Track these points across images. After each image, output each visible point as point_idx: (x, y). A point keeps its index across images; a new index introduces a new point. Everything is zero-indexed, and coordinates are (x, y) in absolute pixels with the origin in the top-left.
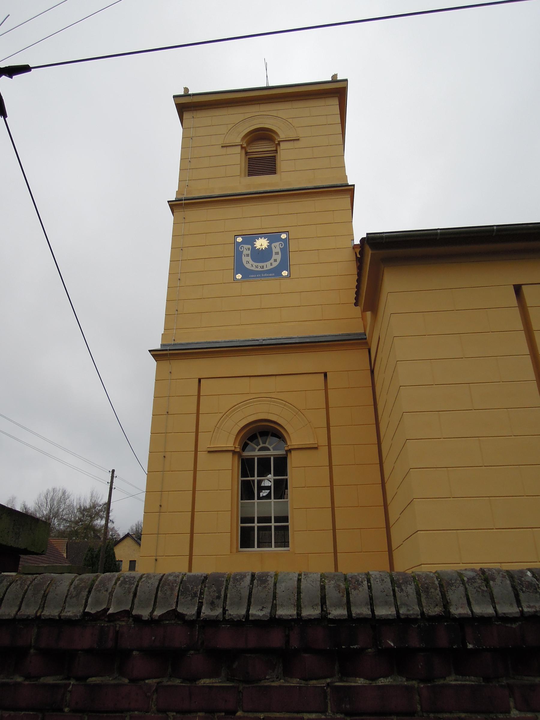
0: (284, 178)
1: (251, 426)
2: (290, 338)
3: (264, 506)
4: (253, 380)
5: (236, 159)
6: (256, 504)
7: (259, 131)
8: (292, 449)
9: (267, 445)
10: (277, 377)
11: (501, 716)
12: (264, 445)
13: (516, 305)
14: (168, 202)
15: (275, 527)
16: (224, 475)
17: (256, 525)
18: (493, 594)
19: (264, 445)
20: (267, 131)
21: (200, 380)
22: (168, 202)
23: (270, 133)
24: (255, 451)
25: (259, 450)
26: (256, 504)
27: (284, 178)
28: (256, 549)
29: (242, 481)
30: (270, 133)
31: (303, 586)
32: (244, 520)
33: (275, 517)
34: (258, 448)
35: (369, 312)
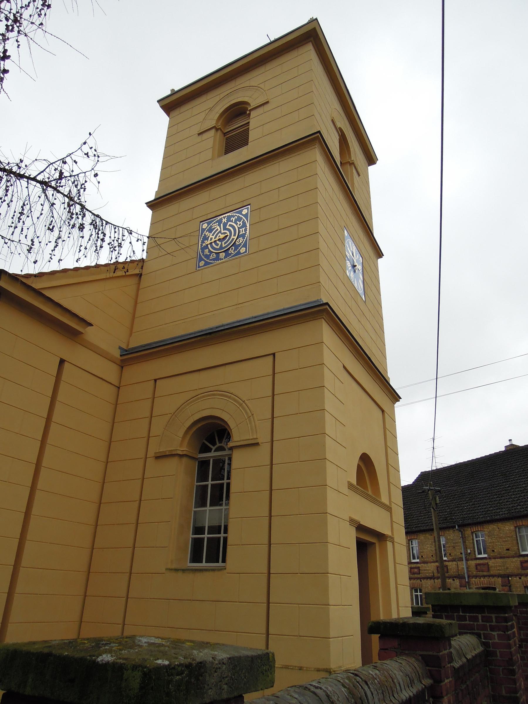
0: (257, 146)
2: (210, 333)
3: (209, 515)
4: (203, 373)
5: (212, 140)
6: (208, 511)
7: (234, 107)
8: (234, 447)
10: (201, 372)
12: (216, 446)
13: (55, 376)
14: (146, 203)
16: (175, 482)
17: (206, 536)
19: (221, 445)
20: (238, 105)
21: (155, 380)
22: (146, 203)
23: (244, 106)
25: (215, 451)
26: (208, 511)
27: (257, 146)
29: (197, 486)
30: (244, 106)
31: (173, 567)
33: (208, 527)
34: (214, 448)
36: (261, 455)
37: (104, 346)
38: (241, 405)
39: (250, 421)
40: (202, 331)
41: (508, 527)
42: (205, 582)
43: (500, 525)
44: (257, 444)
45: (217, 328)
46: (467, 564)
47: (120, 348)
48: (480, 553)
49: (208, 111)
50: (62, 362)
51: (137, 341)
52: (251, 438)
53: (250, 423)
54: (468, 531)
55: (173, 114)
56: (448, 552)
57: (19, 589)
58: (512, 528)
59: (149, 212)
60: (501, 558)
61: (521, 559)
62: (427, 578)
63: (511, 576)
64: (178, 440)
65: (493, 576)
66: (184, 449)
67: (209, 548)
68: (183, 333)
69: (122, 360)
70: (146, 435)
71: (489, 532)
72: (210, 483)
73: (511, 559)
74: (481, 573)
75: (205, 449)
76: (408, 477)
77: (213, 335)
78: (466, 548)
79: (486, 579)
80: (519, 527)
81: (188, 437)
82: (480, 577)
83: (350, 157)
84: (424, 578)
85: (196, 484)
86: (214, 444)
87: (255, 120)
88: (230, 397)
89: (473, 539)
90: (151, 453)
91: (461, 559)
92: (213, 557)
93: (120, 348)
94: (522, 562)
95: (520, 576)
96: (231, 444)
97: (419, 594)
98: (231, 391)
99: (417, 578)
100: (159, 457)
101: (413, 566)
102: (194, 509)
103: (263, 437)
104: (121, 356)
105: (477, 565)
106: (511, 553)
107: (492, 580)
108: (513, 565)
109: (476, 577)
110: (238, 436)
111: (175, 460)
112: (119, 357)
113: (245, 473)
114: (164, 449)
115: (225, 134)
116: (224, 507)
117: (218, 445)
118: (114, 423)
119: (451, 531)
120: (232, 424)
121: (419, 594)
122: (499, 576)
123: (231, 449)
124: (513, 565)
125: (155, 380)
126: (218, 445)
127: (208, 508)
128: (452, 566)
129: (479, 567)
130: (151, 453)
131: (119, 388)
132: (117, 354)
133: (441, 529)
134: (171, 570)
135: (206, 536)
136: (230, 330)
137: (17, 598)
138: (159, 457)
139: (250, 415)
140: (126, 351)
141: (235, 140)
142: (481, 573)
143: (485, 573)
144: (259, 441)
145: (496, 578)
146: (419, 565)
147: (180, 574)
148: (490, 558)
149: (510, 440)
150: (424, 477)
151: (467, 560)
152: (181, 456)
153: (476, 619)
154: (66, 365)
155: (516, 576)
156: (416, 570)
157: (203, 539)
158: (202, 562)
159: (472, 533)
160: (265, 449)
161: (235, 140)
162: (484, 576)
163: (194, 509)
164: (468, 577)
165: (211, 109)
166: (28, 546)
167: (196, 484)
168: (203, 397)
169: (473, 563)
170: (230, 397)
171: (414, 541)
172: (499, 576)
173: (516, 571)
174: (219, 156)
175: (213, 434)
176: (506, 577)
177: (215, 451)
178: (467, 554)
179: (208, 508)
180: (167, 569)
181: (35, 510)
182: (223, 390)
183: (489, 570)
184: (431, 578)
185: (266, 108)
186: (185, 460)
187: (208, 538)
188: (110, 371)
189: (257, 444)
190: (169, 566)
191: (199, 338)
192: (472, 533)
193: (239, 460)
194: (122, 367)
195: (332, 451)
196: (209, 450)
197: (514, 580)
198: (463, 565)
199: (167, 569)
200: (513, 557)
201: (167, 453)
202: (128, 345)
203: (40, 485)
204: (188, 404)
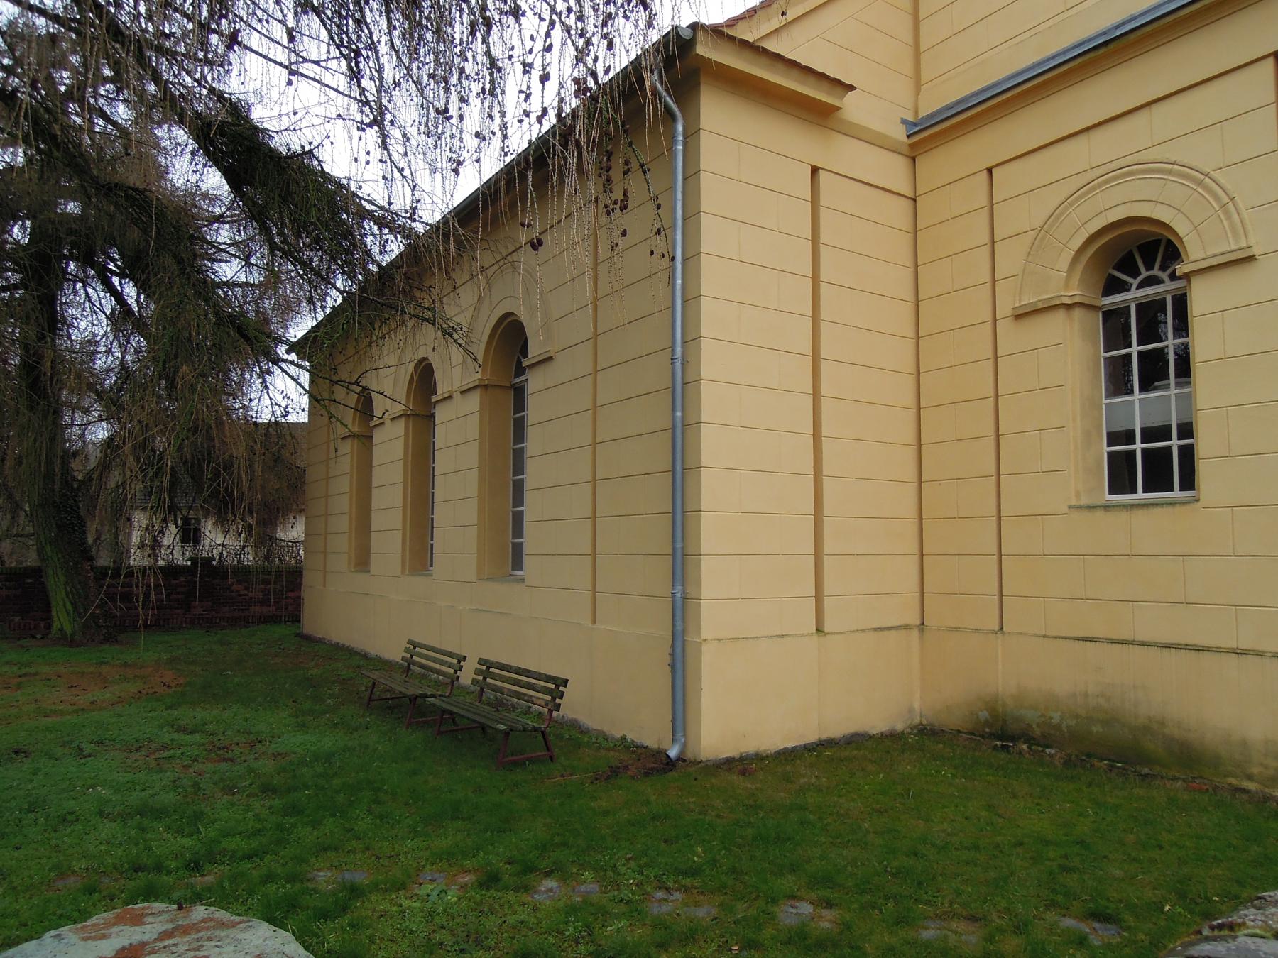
1: (1146, 228)
3: (1139, 408)
6: (1137, 402)
9: (1156, 272)
11: (1218, 948)
12: (1140, 278)
15: (1170, 448)
16: (1066, 356)
17: (1139, 446)
18: (18, 944)
19: (1140, 278)
21: (990, 171)
24: (1129, 290)
25: (1140, 286)
26: (1137, 402)
28: (1140, 495)
31: (1084, 501)
32: (1113, 438)
33: (1179, 426)
34: (1135, 282)
35: (306, 420)
37: (876, 125)
38: (1200, 183)
39: (1227, 213)
40: (1081, 44)
42: (1153, 521)
44: (1251, 258)
45: (1117, 27)
47: (904, 122)
50: (815, 170)
51: (932, 103)
52: (1233, 247)
53: (1229, 217)
57: (828, 547)
64: (1061, 277)
66: (1074, 292)
67: (1153, 465)
68: (1036, 59)
69: (912, 146)
70: (988, 278)
71: (239, 582)
72: (1135, 349)
75: (1113, 286)
77: (1111, 47)
81: (1080, 267)
85: (1103, 355)
86: (1135, 273)
88: (1170, 172)
90: (1004, 309)
92: (1158, 478)
93: (904, 122)
96: (1182, 269)
98: (1173, 159)
100: (1021, 316)
102: (1105, 401)
104: (908, 136)
110: (1195, 252)
111: (1061, 315)
112: (905, 139)
114: (1029, 299)
116: (1173, 391)
117: (1156, 272)
118: (916, 266)
120: (1181, 227)
123: (1187, 276)
125: (990, 171)
126: (1144, 274)
127: (1137, 396)
131: (915, 200)
132: (900, 134)
134: (1080, 507)
135: (1139, 446)
136: (1155, 25)
138: (1021, 316)
139: (1226, 199)
140: (915, 125)
144: (1256, 251)
147: (1100, 514)
152: (1069, 307)
154: (823, 175)
157: (1133, 452)
158: (1136, 492)
163: (1105, 401)
167: (1103, 355)
168: (1106, 182)
170: (1170, 172)
175: (1138, 252)
177: (1138, 288)
179: (1137, 396)
180: (1070, 507)
182: (1151, 158)
186: (1078, 313)
187: (1144, 451)
188: (893, 171)
189: (1251, 258)
190: (1074, 502)
191: (1079, 60)
193: (1204, 299)
194: (914, 159)
196: (1124, 287)
199: (1070, 507)
201: (1041, 305)
202: (916, 112)
204: (1071, 205)
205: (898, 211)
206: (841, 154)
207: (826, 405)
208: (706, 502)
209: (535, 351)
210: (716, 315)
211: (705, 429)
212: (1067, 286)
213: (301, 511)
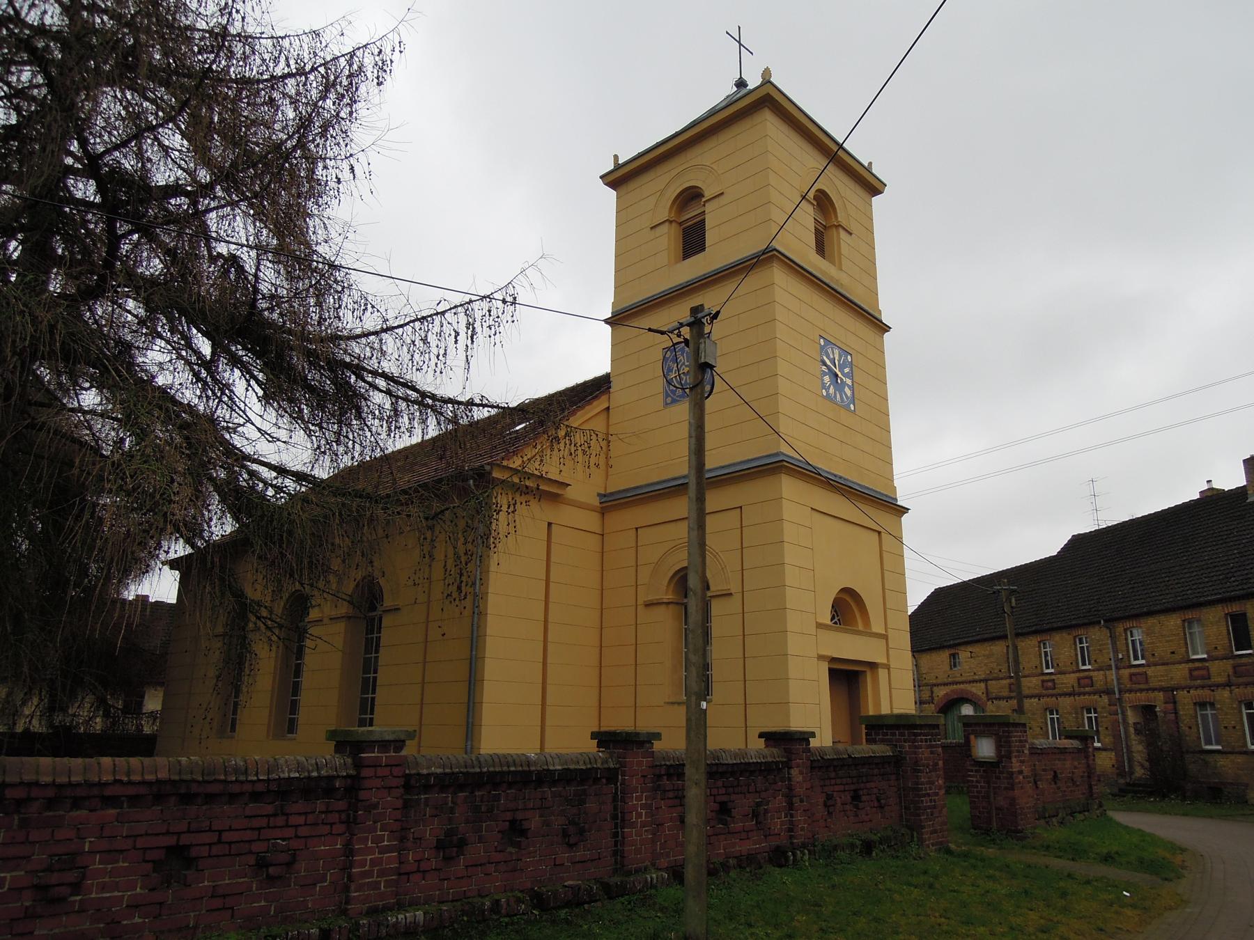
16: (662, 630)
36: (734, 604)
41: (1173, 622)
43: (1162, 618)
46: (1117, 674)
47: (599, 495)
48: (1136, 658)
49: (660, 190)
50: (550, 524)
51: (617, 484)
54: (1120, 628)
55: (624, 189)
56: (1093, 658)
57: (548, 723)
58: (1179, 622)
59: (612, 194)
60: (1163, 664)
61: (1191, 665)
62: (1065, 694)
63: (1177, 689)
65: (1154, 690)
66: (670, 597)
73: (1177, 666)
74: (1138, 686)
76: (915, 598)
78: (1116, 652)
79: (1144, 694)
80: (1190, 622)
82: (1084, 694)
83: (836, 217)
84: (1061, 695)
87: (714, 218)
89: (1126, 639)
91: (1109, 668)
93: (599, 495)
94: (1191, 670)
95: (1188, 688)
97: (1093, 715)
99: (1052, 696)
100: (649, 605)
101: (1082, 675)
103: (734, 587)
105: (1131, 675)
106: (1177, 657)
107: (1152, 695)
108: (1179, 673)
109: (1130, 691)
111: (663, 608)
113: (723, 619)
115: (680, 224)
119: (1097, 627)
121: (1093, 715)
122: (1161, 689)
124: (1179, 673)
128: (1098, 676)
129: (1082, 682)
130: (640, 602)
132: (595, 502)
133: (1018, 635)
137: (547, 729)
138: (649, 605)
141: (693, 240)
142: (1138, 686)
143: (1142, 686)
145: (1156, 693)
146: (1092, 674)
148: (1148, 665)
149: (1209, 482)
150: (940, 597)
151: (1118, 668)
153: (894, 734)
155: (1183, 689)
156: (1050, 684)
159: (1125, 630)
160: (737, 598)
161: (693, 240)
162: (1141, 690)
164: (1120, 692)
165: (662, 192)
166: (550, 689)
169: (1125, 673)
171: (1135, 631)
172: (1161, 689)
173: (1183, 683)
174: (677, 262)
176: (1170, 691)
178: (1117, 660)
181: (549, 660)
183: (1147, 682)
184: (1070, 695)
185: (723, 200)
186: (671, 606)
188: (591, 521)
192: (1125, 630)
195: (793, 598)
197: (1181, 695)
198: (1112, 675)
200: (1180, 663)
203: (550, 638)
205: (594, 541)
206: (564, 515)
207: (550, 647)
208: (490, 610)
209: (388, 603)
210: (494, 626)
211: (487, 660)
212: (667, 593)
213: (162, 684)
